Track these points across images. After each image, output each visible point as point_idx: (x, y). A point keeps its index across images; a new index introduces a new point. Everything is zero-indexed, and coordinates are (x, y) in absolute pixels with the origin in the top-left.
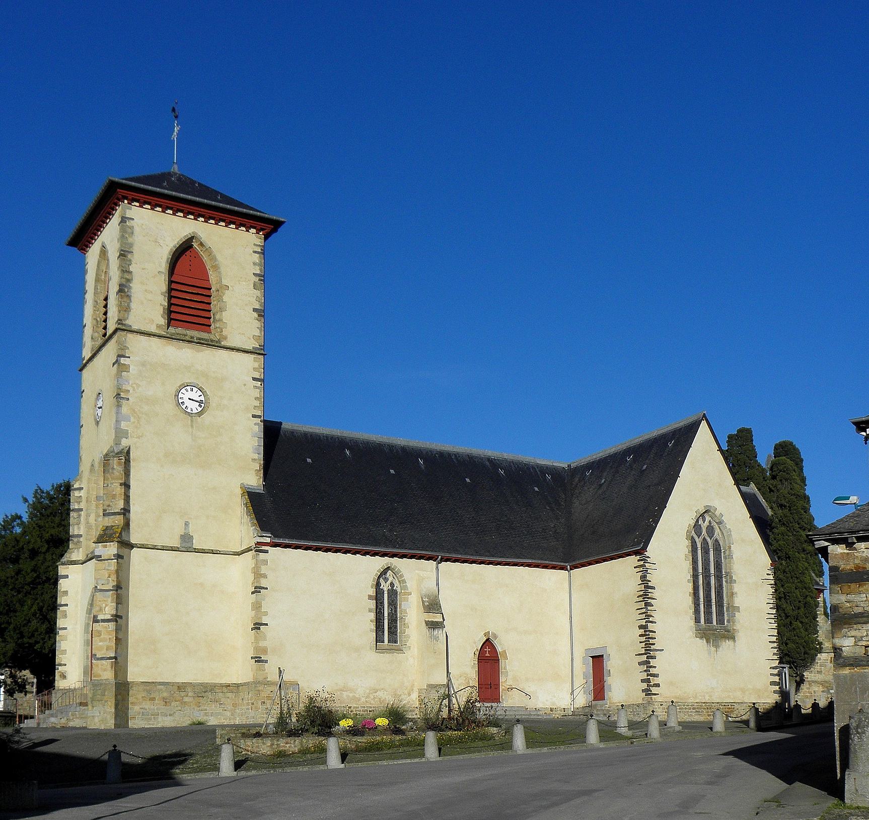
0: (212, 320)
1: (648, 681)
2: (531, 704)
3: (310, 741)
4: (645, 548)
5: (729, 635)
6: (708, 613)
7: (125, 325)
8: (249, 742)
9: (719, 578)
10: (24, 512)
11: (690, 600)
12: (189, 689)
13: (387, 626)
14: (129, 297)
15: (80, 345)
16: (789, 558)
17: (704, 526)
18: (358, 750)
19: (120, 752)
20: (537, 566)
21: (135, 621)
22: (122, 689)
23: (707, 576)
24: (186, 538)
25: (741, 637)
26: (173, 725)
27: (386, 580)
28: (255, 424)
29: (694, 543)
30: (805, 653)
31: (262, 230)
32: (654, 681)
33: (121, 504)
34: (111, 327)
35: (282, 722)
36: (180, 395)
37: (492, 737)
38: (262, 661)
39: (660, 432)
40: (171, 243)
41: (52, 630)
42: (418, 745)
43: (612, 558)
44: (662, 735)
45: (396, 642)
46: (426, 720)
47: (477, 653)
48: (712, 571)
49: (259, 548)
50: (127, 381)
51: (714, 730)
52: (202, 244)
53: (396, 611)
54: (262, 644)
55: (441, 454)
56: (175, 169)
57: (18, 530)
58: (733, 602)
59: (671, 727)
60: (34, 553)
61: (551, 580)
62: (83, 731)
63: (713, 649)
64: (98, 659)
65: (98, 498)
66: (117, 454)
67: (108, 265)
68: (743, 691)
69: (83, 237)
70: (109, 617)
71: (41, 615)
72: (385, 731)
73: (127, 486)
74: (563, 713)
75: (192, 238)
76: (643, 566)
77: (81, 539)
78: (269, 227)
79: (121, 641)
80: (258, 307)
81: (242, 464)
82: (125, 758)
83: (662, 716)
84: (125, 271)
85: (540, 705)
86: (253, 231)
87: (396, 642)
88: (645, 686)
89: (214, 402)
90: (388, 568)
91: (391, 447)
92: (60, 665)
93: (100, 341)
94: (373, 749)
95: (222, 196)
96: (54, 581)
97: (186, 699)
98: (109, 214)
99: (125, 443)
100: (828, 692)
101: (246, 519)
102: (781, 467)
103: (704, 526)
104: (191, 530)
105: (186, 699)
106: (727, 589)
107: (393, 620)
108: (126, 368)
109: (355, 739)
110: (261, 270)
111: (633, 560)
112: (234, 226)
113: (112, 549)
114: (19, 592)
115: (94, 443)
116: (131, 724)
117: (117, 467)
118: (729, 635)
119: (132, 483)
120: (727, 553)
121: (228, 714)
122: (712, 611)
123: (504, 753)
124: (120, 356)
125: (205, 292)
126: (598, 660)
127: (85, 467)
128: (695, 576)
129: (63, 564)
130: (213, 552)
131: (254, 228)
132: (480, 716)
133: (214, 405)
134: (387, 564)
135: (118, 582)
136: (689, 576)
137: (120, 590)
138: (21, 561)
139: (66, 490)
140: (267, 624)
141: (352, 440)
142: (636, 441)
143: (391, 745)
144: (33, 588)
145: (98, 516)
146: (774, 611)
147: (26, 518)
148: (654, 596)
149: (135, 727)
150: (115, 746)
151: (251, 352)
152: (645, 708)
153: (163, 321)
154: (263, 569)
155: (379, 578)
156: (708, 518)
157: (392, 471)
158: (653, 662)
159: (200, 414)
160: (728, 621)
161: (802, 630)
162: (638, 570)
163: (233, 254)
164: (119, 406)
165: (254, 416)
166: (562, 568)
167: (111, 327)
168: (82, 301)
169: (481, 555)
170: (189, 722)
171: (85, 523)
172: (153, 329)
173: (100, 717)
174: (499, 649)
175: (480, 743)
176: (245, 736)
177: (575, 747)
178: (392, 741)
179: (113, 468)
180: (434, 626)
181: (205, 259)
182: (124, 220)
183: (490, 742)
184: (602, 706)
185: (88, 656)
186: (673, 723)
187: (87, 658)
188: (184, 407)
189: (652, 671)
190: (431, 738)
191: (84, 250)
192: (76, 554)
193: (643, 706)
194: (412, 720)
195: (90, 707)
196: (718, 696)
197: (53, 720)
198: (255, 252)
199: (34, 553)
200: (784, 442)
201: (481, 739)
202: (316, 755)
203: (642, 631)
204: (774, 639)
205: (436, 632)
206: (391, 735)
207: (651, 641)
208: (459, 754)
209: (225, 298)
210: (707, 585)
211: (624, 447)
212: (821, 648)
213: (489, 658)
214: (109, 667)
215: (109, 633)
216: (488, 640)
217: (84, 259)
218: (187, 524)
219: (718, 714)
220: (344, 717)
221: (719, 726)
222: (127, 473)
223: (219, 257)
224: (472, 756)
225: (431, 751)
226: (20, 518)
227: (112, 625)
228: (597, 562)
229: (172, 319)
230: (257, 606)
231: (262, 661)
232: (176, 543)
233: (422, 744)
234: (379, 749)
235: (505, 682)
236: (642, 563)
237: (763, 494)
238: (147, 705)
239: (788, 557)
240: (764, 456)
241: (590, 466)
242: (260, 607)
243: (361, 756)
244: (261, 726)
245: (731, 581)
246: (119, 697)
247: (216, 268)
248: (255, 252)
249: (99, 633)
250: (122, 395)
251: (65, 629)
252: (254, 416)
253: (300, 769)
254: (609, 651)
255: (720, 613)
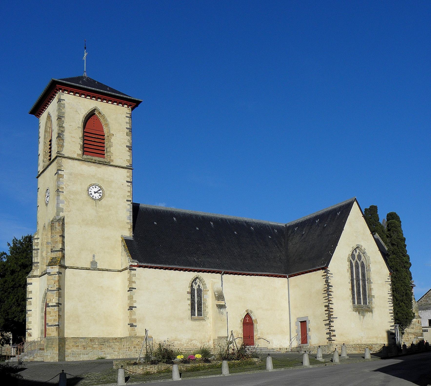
0: (105, 151)
1: (330, 333)
2: (270, 346)
3: (163, 367)
4: (327, 266)
5: (370, 310)
6: (359, 299)
7: (60, 154)
8: (131, 368)
9: (364, 281)
10: (7, 250)
11: (350, 292)
12: (96, 341)
13: (197, 307)
14: (63, 140)
15: (37, 165)
16: (398, 270)
17: (356, 255)
18: (187, 371)
19: (65, 374)
20: (272, 276)
21: (68, 306)
22: (62, 341)
23: (358, 280)
24: (94, 263)
25: (375, 310)
26: (88, 359)
27: (196, 284)
28: (128, 205)
29: (351, 263)
30: (406, 319)
31: (130, 105)
32: (333, 333)
33: (60, 246)
34: (54, 155)
35: (147, 357)
36: (90, 190)
37: (254, 363)
38: (134, 326)
39: (333, 208)
40: (84, 112)
41: (23, 311)
42: (218, 368)
43: (310, 272)
44: (340, 361)
45: (201, 315)
46: (221, 355)
47: (242, 321)
48: (361, 278)
49: (131, 268)
50: (63, 183)
51: (366, 358)
52: (100, 113)
53: (201, 300)
54: (133, 317)
55: (222, 219)
56: (85, 74)
57: (5, 260)
58: (371, 293)
59: (343, 357)
60: (13, 272)
61: (279, 283)
62: (43, 363)
63: (362, 317)
64: (49, 326)
65: (47, 243)
66: (58, 220)
67: (51, 123)
68: (377, 338)
69: (38, 109)
70: (55, 304)
71: (17, 303)
72: (200, 361)
73: (63, 236)
74: (286, 350)
75: (95, 109)
76: (326, 275)
77: (39, 264)
78: (134, 104)
79: (61, 317)
80: (129, 145)
81: (122, 225)
82: (68, 377)
83: (340, 351)
84: (61, 126)
85: (274, 347)
86: (126, 106)
87: (201, 315)
88: (328, 336)
89: (107, 193)
90: (197, 278)
91: (197, 216)
92: (28, 329)
93: (47, 163)
94: (195, 370)
95: (110, 88)
96: (25, 285)
97: (95, 346)
98: (52, 98)
99: (61, 214)
100: (417, 338)
101: (124, 253)
102: (393, 225)
103: (356, 255)
104: (96, 259)
105: (95, 346)
106: (368, 286)
107: (200, 304)
108: (62, 176)
109: (186, 365)
110: (130, 126)
111: (321, 272)
112: (116, 104)
113: (56, 269)
114: (6, 292)
115: (45, 215)
116: (67, 359)
117: (58, 226)
118: (370, 310)
119: (66, 235)
120: (368, 268)
121: (116, 353)
122: (361, 299)
123: (262, 371)
124: (58, 170)
125: (102, 137)
126: (303, 324)
127: (40, 227)
128: (352, 280)
129: (29, 277)
130: (107, 270)
131: (126, 104)
132: (248, 352)
133: (107, 195)
134: (196, 276)
135: (59, 286)
136: (349, 280)
137: (60, 290)
138: (6, 276)
139: (29, 240)
140: (136, 307)
141: (176, 212)
142: (321, 212)
143: (204, 368)
144: (13, 290)
145: (47, 252)
146: (392, 298)
147: (9, 254)
148: (332, 290)
149: (69, 360)
150: (63, 371)
151: (126, 168)
152: (328, 347)
153: (80, 152)
154: (134, 279)
155: (192, 283)
156: (358, 251)
157: (197, 228)
158: (332, 324)
159: (100, 200)
160: (369, 303)
161: (405, 307)
162: (324, 277)
163: (116, 118)
164: (58, 196)
165: (127, 201)
166: (285, 277)
167: (54, 155)
168: (38, 143)
169: (243, 271)
170: (97, 358)
171: (41, 256)
172: (75, 156)
173: (51, 356)
174: (253, 318)
175: (249, 367)
176: (129, 364)
177: (297, 368)
178: (204, 366)
179: (56, 228)
180: (221, 307)
181: (102, 120)
182: (60, 100)
183: (254, 366)
184: (306, 346)
185: (43, 324)
186: (344, 355)
187: (43, 326)
188: (92, 196)
189: (332, 328)
190: (225, 364)
191: (38, 116)
192: (36, 272)
193: (328, 347)
194: (212, 355)
195: (45, 351)
196: (364, 341)
197: (26, 357)
198: (127, 117)
199: (13, 272)
200: (392, 213)
201: (249, 364)
202: (166, 374)
203: (326, 308)
204: (392, 312)
205: (222, 310)
206: (204, 362)
207: (331, 313)
208: (239, 372)
209: (112, 140)
210: (358, 285)
211: (314, 215)
212: (414, 316)
213: (248, 323)
214: (55, 330)
215: (55, 312)
216: (248, 314)
217: (39, 121)
218: (94, 256)
219: (368, 350)
220: (181, 354)
221: (368, 356)
222: (63, 230)
223: (108, 119)
224: (248, 373)
225: (225, 370)
226: (5, 254)
227: (56, 308)
228: (303, 273)
229: (85, 151)
230: (131, 298)
231: (134, 326)
232: (89, 266)
233: (220, 367)
234: (198, 370)
235: (257, 334)
236: (326, 274)
237: (382, 239)
238: (75, 349)
239: (397, 270)
240: (382, 218)
241: (297, 225)
242: (132, 298)
243: (189, 374)
244: (137, 359)
245: (370, 282)
246: (61, 345)
247: (107, 125)
248: (127, 117)
249: (50, 312)
250: (60, 190)
251: (31, 310)
252: (127, 201)
253: (159, 381)
254: (309, 318)
255: (365, 299)
